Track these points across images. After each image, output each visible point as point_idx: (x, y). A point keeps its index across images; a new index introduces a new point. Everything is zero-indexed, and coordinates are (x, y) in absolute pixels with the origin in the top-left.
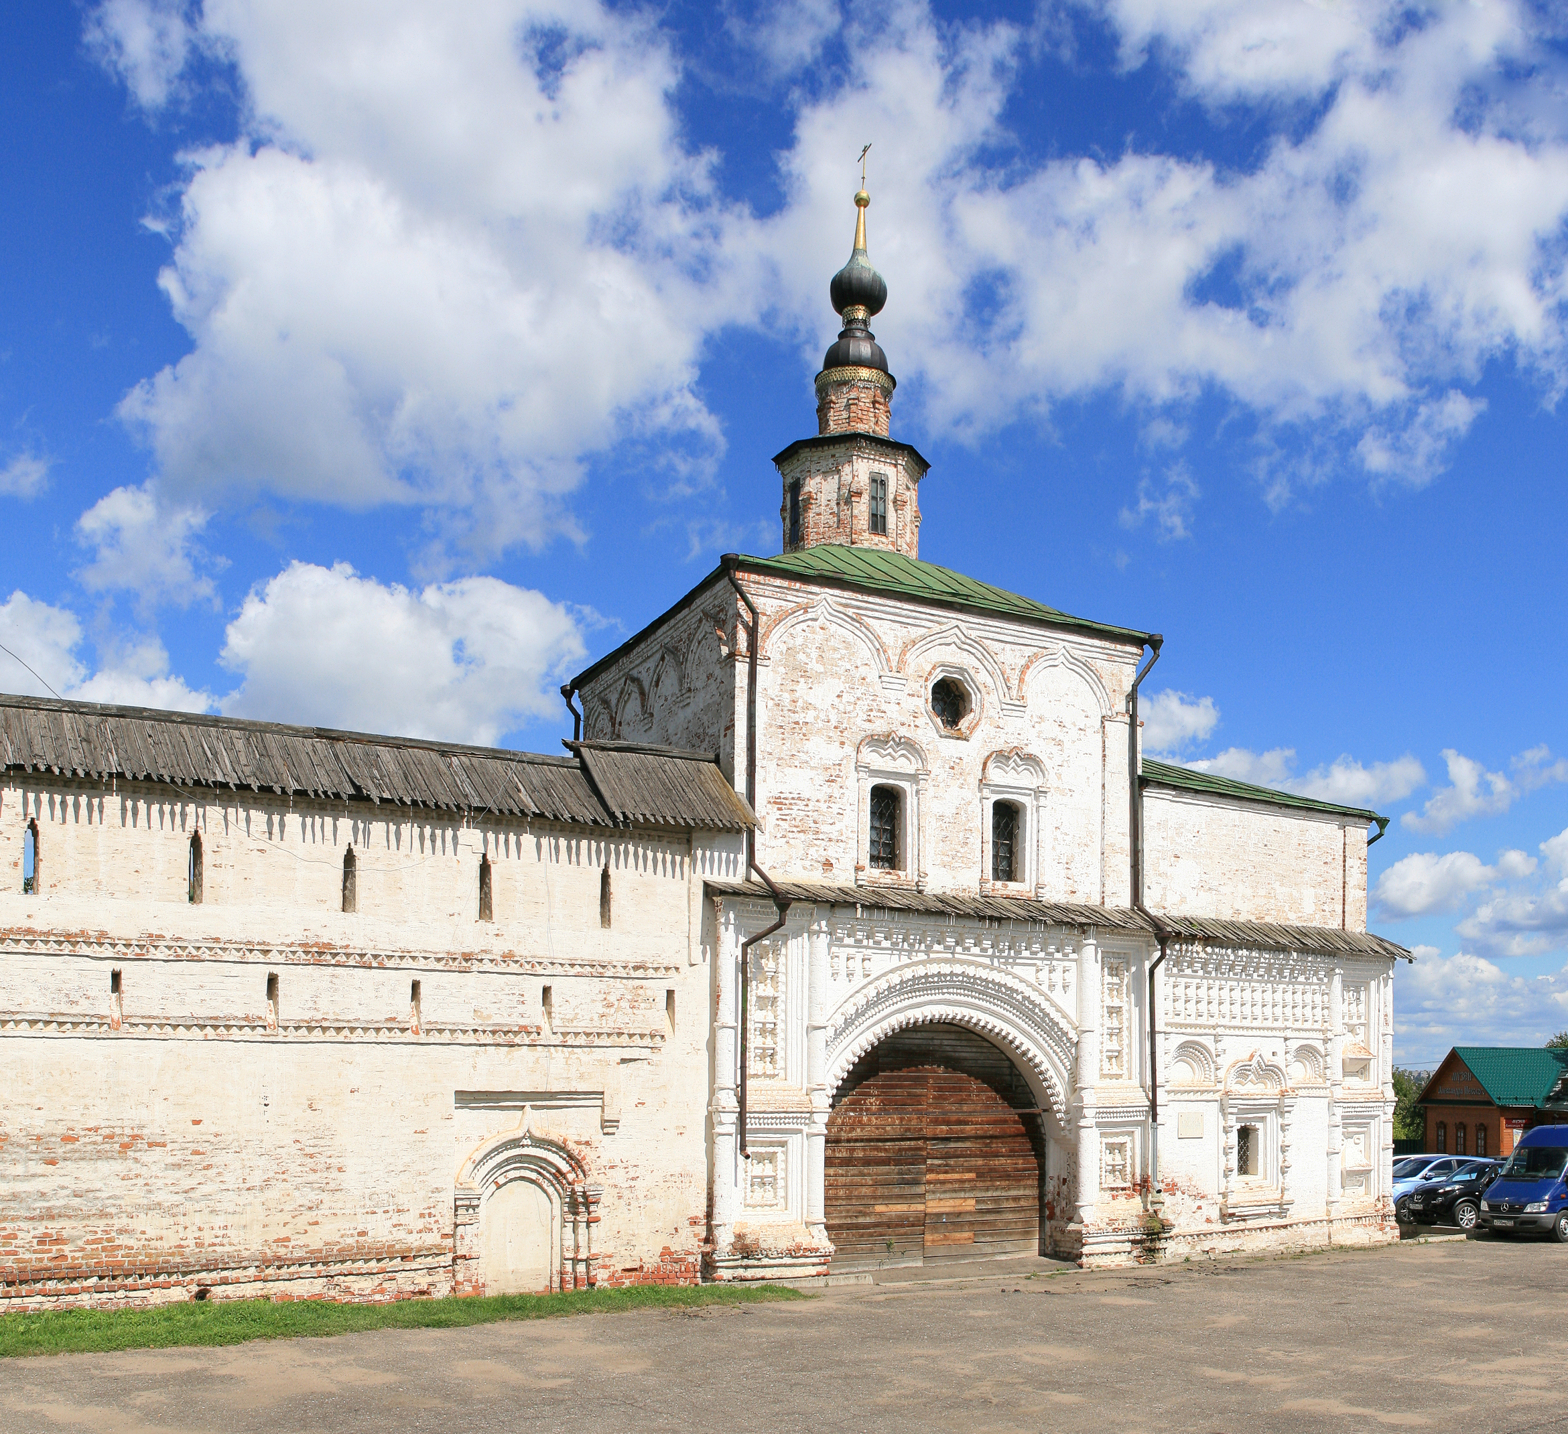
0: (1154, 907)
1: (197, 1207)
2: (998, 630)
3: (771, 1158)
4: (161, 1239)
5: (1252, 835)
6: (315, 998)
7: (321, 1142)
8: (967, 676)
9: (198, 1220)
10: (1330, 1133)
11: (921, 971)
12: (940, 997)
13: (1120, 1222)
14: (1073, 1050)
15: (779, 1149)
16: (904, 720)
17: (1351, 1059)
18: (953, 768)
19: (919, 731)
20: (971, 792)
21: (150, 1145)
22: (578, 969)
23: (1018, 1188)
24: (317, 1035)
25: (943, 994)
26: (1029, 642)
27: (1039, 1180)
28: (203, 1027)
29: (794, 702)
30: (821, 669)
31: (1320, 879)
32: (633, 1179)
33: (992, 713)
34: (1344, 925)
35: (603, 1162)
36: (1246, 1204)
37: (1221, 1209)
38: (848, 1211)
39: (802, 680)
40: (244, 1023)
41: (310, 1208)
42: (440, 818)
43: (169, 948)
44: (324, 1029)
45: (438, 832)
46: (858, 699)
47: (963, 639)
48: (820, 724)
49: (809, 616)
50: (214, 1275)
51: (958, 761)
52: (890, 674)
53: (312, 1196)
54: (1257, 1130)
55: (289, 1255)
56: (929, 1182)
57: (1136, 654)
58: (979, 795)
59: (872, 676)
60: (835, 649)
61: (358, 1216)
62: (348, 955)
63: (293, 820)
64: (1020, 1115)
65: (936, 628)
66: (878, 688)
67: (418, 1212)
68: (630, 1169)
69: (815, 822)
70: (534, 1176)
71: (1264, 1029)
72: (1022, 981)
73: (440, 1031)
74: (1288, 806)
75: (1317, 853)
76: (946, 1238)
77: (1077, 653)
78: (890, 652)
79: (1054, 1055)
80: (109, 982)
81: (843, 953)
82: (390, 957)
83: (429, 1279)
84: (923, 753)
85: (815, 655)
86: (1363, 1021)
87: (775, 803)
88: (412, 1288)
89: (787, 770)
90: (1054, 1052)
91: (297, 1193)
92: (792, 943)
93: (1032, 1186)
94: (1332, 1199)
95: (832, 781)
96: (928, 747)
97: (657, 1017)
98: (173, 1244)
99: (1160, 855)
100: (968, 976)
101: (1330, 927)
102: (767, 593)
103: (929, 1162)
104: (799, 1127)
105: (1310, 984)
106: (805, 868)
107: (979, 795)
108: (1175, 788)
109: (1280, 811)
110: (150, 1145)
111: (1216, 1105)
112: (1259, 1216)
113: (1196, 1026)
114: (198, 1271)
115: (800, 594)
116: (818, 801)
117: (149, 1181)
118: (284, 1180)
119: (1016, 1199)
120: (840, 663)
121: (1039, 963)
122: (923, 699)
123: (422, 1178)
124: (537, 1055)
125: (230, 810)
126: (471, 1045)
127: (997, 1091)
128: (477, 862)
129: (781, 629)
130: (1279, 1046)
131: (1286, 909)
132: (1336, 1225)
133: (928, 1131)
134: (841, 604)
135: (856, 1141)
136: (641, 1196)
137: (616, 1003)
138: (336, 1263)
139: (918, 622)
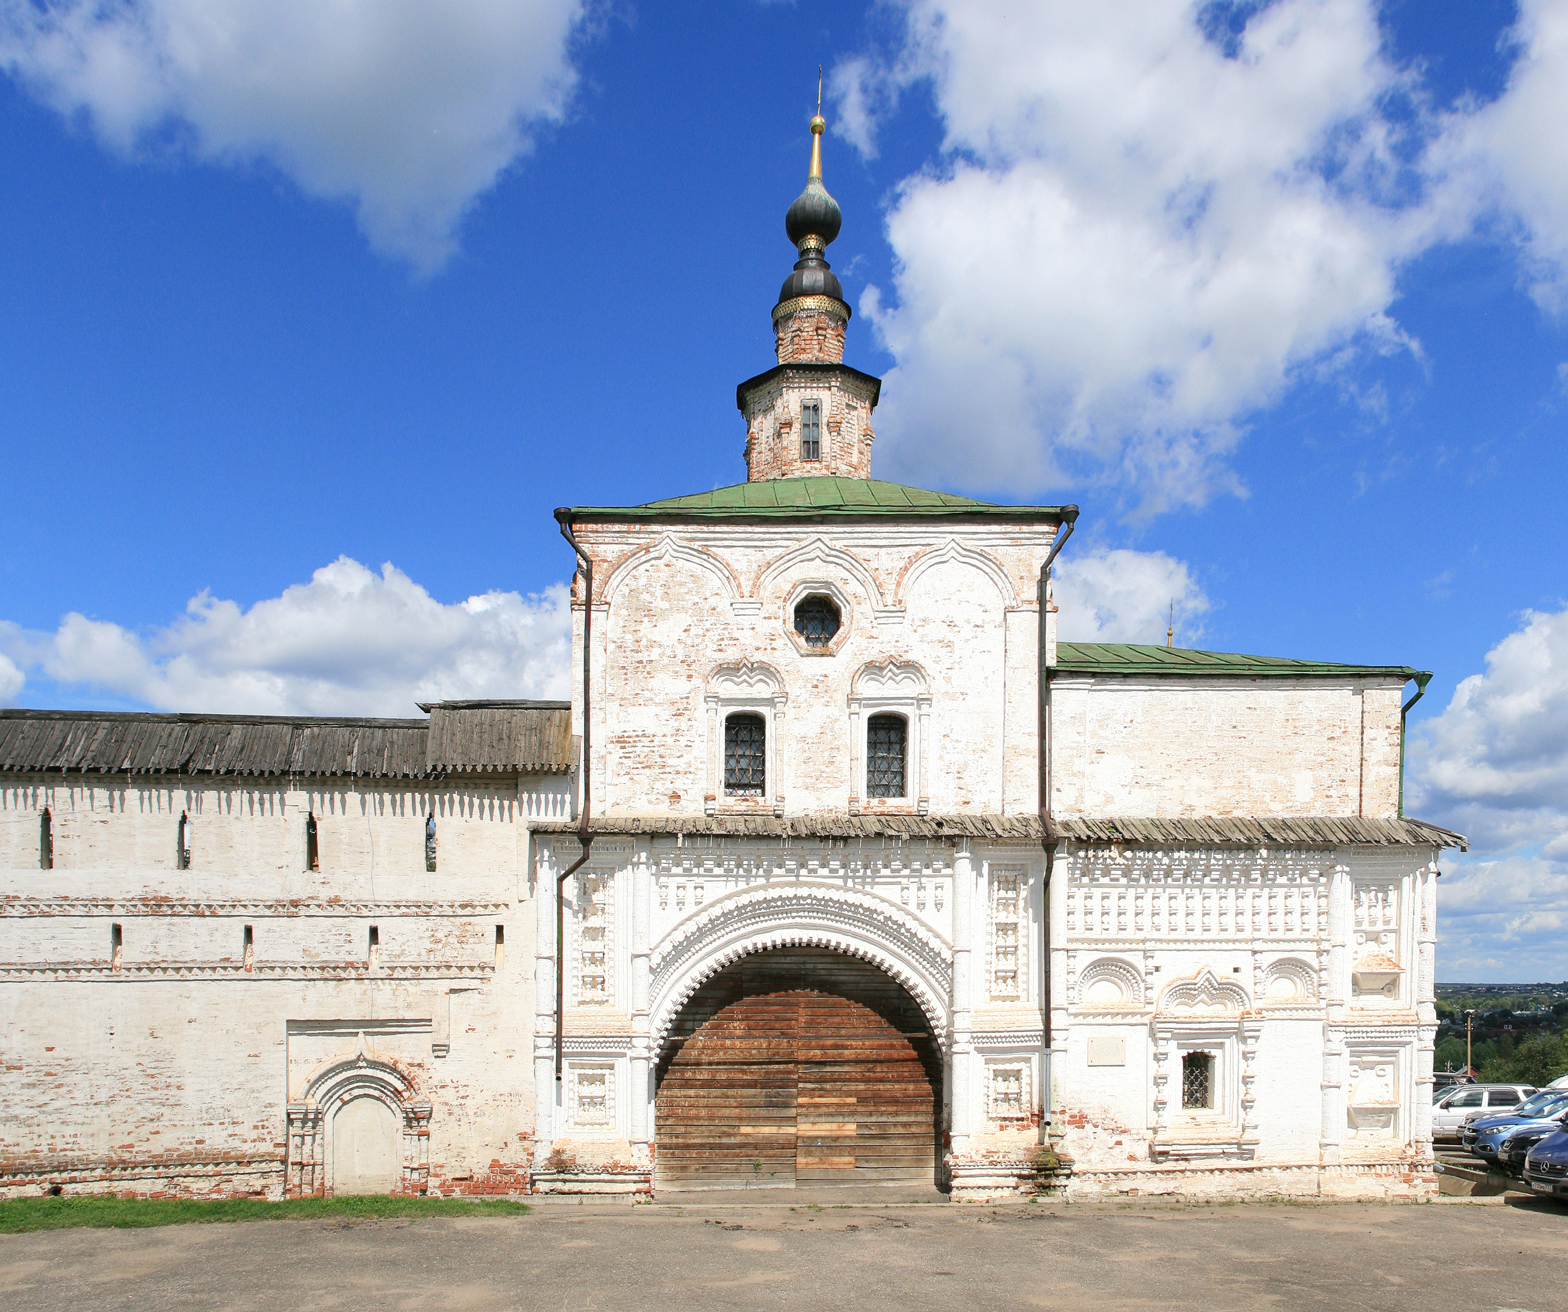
0: (1066, 811)
1: (50, 1118)
2: (869, 535)
3: (602, 1080)
4: (18, 1145)
5: (1213, 717)
6: (155, 943)
7: (162, 1065)
8: (834, 589)
9: (51, 1129)
10: (1325, 1062)
11: (759, 896)
12: (790, 920)
13: (1001, 1155)
14: (950, 972)
15: (607, 1072)
16: (758, 644)
17: (1361, 974)
18: (816, 686)
19: (776, 654)
20: (838, 709)
21: (8, 1068)
22: (404, 910)
23: (909, 1113)
24: (159, 974)
25: (794, 918)
26: (909, 542)
27: (934, 1106)
28: (55, 971)
29: (637, 641)
30: (665, 605)
31: (1321, 759)
32: (463, 1097)
33: (864, 623)
34: (1360, 811)
35: (435, 1081)
36: (1185, 1142)
37: (1150, 1146)
38: (711, 1131)
39: (646, 619)
40: (91, 966)
41: (152, 1120)
42: (268, 783)
43: (25, 906)
44: (165, 970)
45: (266, 796)
46: (707, 630)
47: (827, 551)
48: (666, 660)
49: (652, 555)
50: (65, 1175)
51: (822, 678)
52: (741, 600)
53: (154, 1110)
54: (1214, 1057)
55: (133, 1159)
56: (801, 1106)
57: (1048, 533)
58: (847, 711)
59: (723, 604)
60: (681, 584)
61: (196, 1127)
62: (185, 906)
63: (132, 794)
64: (910, 1040)
65: (795, 545)
66: (730, 616)
67: (252, 1124)
68: (460, 1088)
69: (661, 757)
70: (377, 1093)
72: (883, 900)
73: (272, 968)
75: (1317, 727)
76: (821, 1162)
77: (969, 544)
78: (742, 579)
79: (930, 978)
80: (242, 935)
81: (673, 882)
82: (222, 907)
83: (263, 1182)
84: (778, 676)
85: (659, 592)
86: (1393, 926)
87: (618, 742)
88: (247, 1189)
89: (631, 709)
90: (930, 973)
91: (139, 1108)
92: (618, 875)
93: (926, 1113)
94: (1325, 1141)
95: (680, 715)
96: (787, 668)
97: (485, 949)
98: (29, 1149)
100: (815, 898)
101: (1340, 815)
102: (607, 540)
103: (801, 1085)
104: (622, 1050)
105: (1299, 886)
106: (650, 802)
107: (847, 711)
108: (1094, 675)
109: (1254, 683)
110: (8, 1068)
111: (1146, 1029)
112: (1208, 1156)
113: (1117, 941)
114: (51, 1172)
115: (641, 536)
116: (664, 736)
117: (8, 1098)
118: (128, 1097)
119: (905, 1125)
120: (687, 597)
121: (904, 881)
122: (781, 620)
123: (255, 1095)
124: (364, 987)
125: (75, 790)
126: (300, 980)
127: (882, 1015)
128: (303, 819)
129: (622, 572)
130: (1245, 961)
131: (1267, 798)
132: (1330, 1172)
133: (801, 1055)
134: (687, 539)
135: (718, 1064)
136: (471, 1113)
137: (444, 939)
138: (176, 1166)
139: (774, 543)
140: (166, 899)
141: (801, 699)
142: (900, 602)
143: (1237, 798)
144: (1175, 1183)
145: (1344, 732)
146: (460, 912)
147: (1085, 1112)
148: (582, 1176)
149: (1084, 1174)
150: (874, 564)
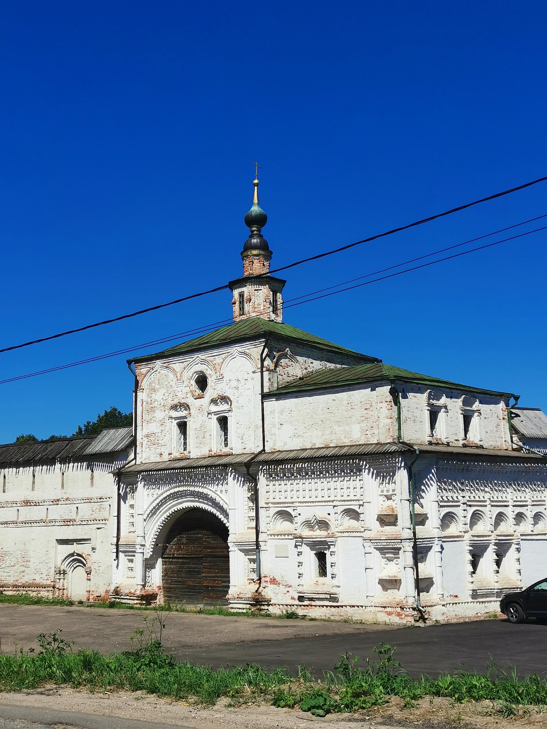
7: (26, 554)
18: (199, 410)
30: (158, 387)
33: (212, 384)
35: (93, 561)
47: (201, 360)
48: (159, 406)
49: (154, 370)
65: (192, 360)
71: (322, 502)
74: (337, 387)
85: (157, 382)
89: (150, 425)
99: (272, 426)
103: (204, 564)
124: (74, 528)
131: (342, 438)
140: (29, 501)
141: (195, 415)
142: (222, 375)
143: (331, 438)
144: (307, 611)
145: (371, 406)
146: (99, 500)
147: (275, 577)
148: (122, 597)
149: (275, 605)
150: (214, 362)
